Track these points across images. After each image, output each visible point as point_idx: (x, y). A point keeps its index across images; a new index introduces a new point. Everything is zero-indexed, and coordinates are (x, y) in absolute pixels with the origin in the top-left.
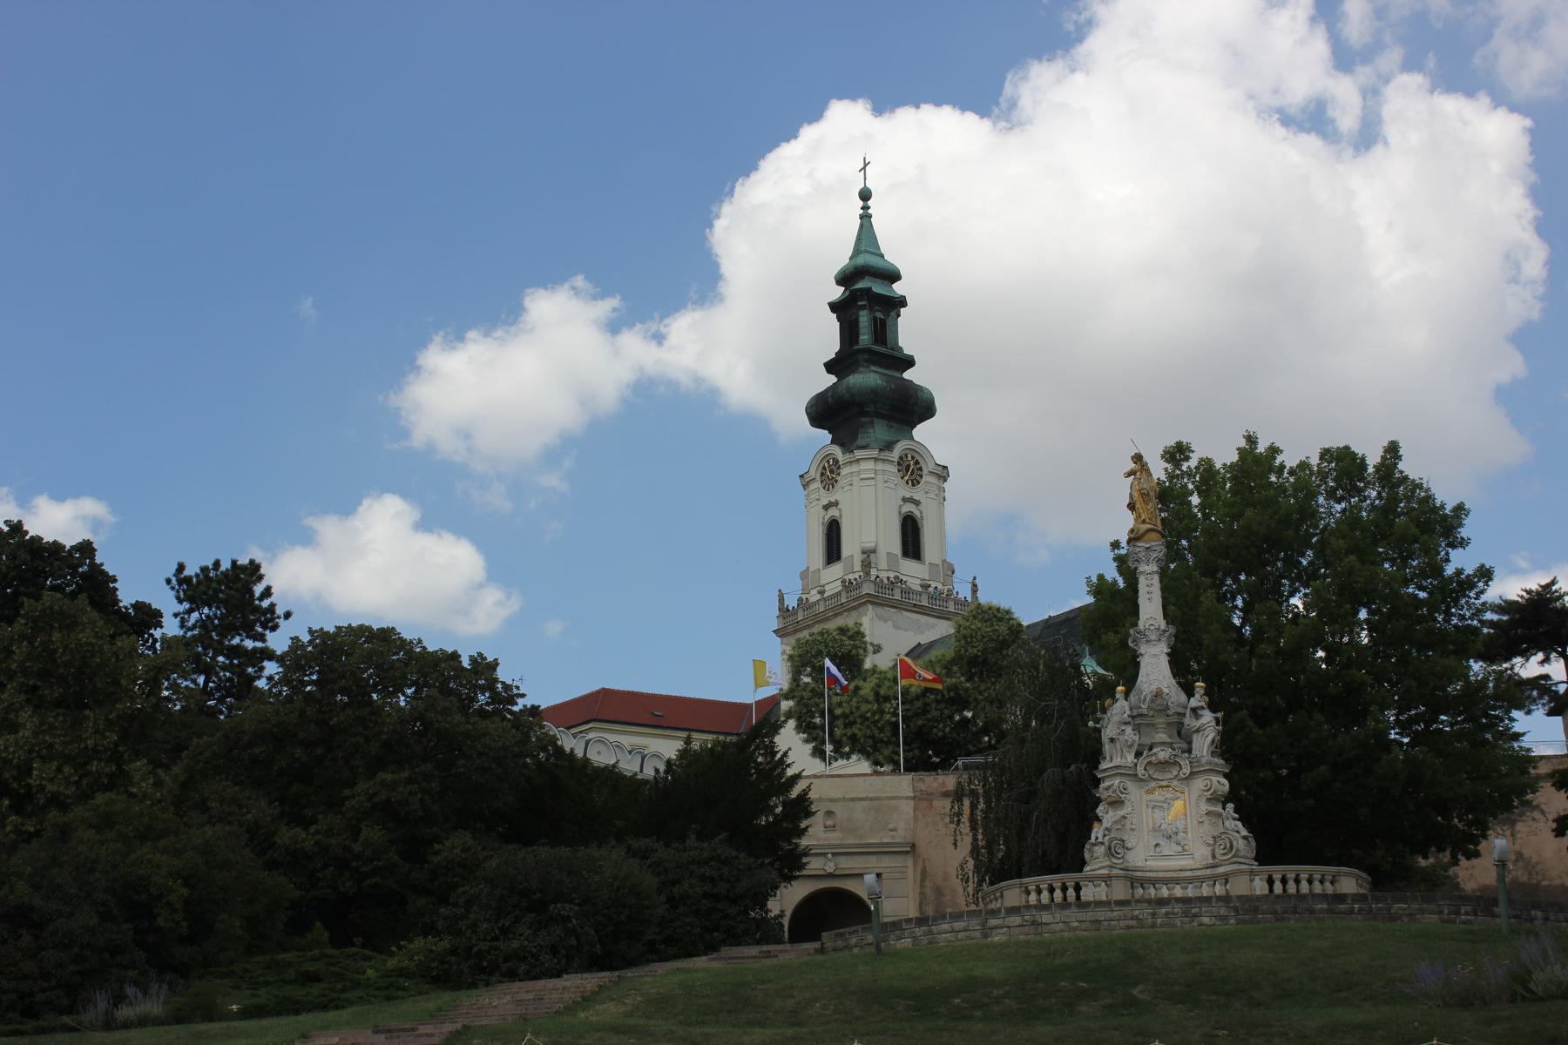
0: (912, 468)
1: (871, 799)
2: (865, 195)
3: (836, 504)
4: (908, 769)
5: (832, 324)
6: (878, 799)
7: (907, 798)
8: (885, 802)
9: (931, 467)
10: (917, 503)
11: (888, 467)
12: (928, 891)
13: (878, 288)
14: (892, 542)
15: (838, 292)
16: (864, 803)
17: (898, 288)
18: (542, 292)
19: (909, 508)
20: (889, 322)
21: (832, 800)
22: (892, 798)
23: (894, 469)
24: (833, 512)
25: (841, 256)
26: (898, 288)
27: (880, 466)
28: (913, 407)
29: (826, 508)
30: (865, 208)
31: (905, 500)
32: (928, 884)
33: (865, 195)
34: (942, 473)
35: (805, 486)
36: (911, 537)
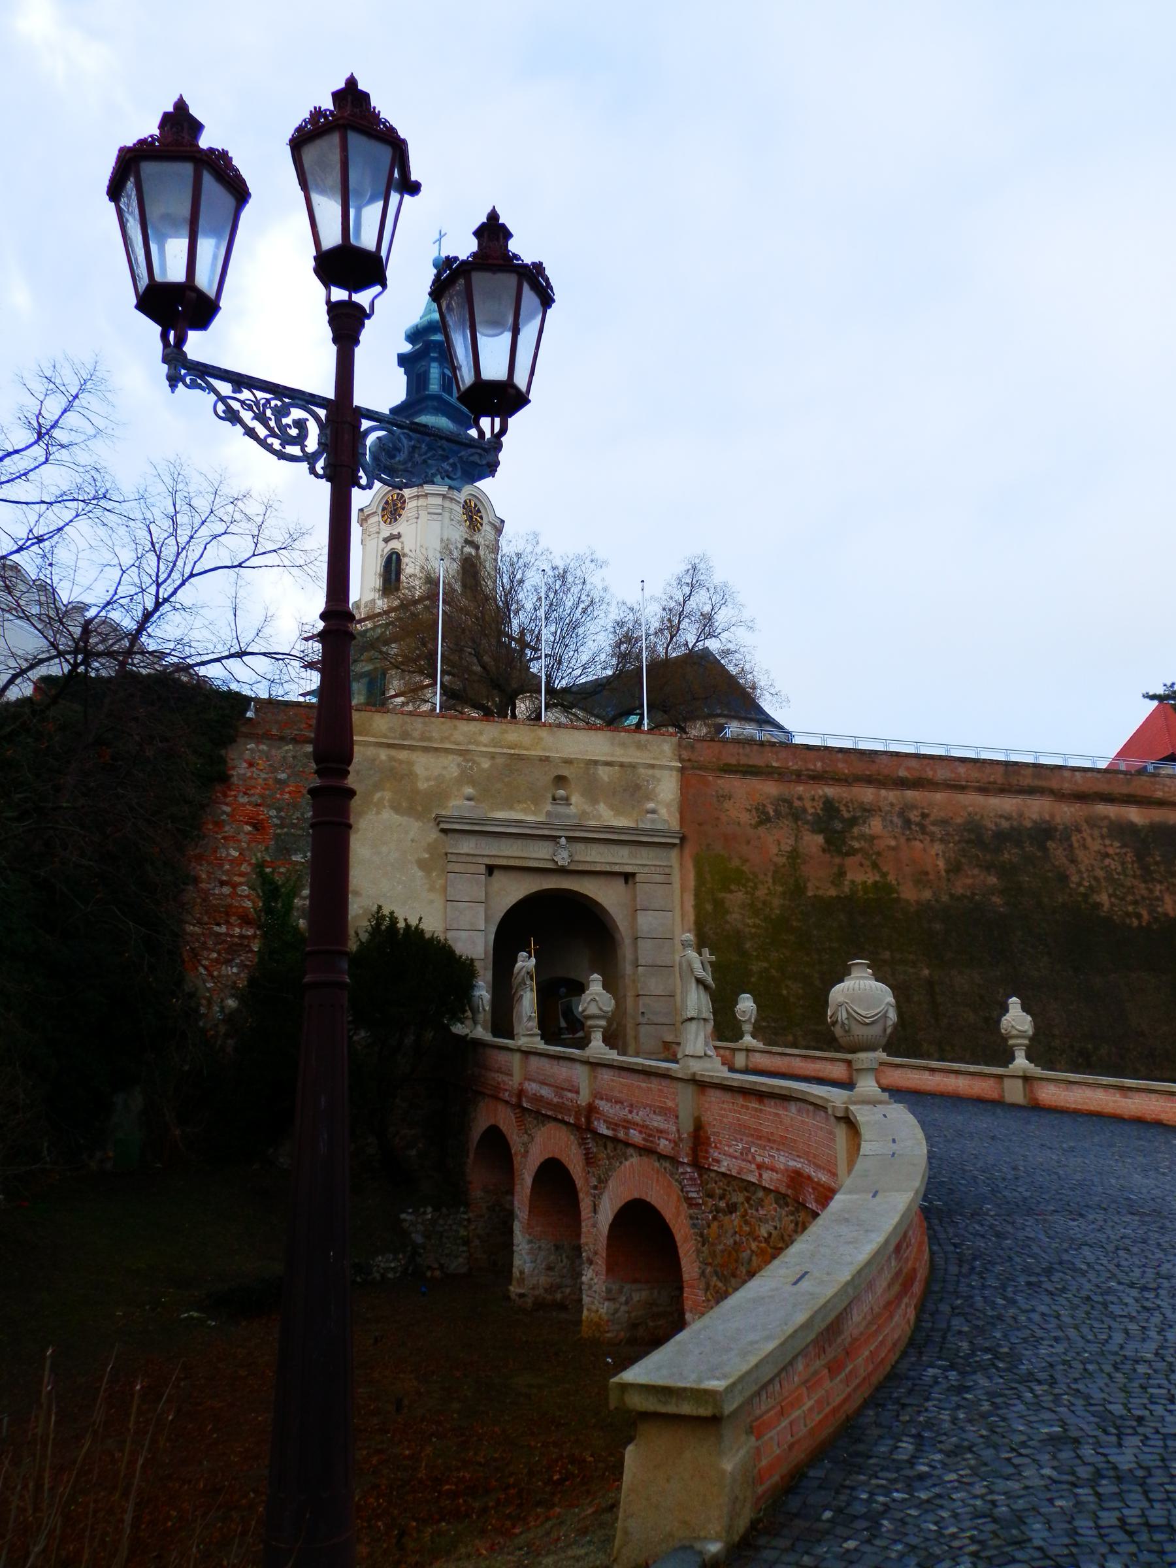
0: (474, 513)
3: (398, 536)
7: (671, 768)
15: (407, 348)
24: (394, 544)
27: (447, 504)
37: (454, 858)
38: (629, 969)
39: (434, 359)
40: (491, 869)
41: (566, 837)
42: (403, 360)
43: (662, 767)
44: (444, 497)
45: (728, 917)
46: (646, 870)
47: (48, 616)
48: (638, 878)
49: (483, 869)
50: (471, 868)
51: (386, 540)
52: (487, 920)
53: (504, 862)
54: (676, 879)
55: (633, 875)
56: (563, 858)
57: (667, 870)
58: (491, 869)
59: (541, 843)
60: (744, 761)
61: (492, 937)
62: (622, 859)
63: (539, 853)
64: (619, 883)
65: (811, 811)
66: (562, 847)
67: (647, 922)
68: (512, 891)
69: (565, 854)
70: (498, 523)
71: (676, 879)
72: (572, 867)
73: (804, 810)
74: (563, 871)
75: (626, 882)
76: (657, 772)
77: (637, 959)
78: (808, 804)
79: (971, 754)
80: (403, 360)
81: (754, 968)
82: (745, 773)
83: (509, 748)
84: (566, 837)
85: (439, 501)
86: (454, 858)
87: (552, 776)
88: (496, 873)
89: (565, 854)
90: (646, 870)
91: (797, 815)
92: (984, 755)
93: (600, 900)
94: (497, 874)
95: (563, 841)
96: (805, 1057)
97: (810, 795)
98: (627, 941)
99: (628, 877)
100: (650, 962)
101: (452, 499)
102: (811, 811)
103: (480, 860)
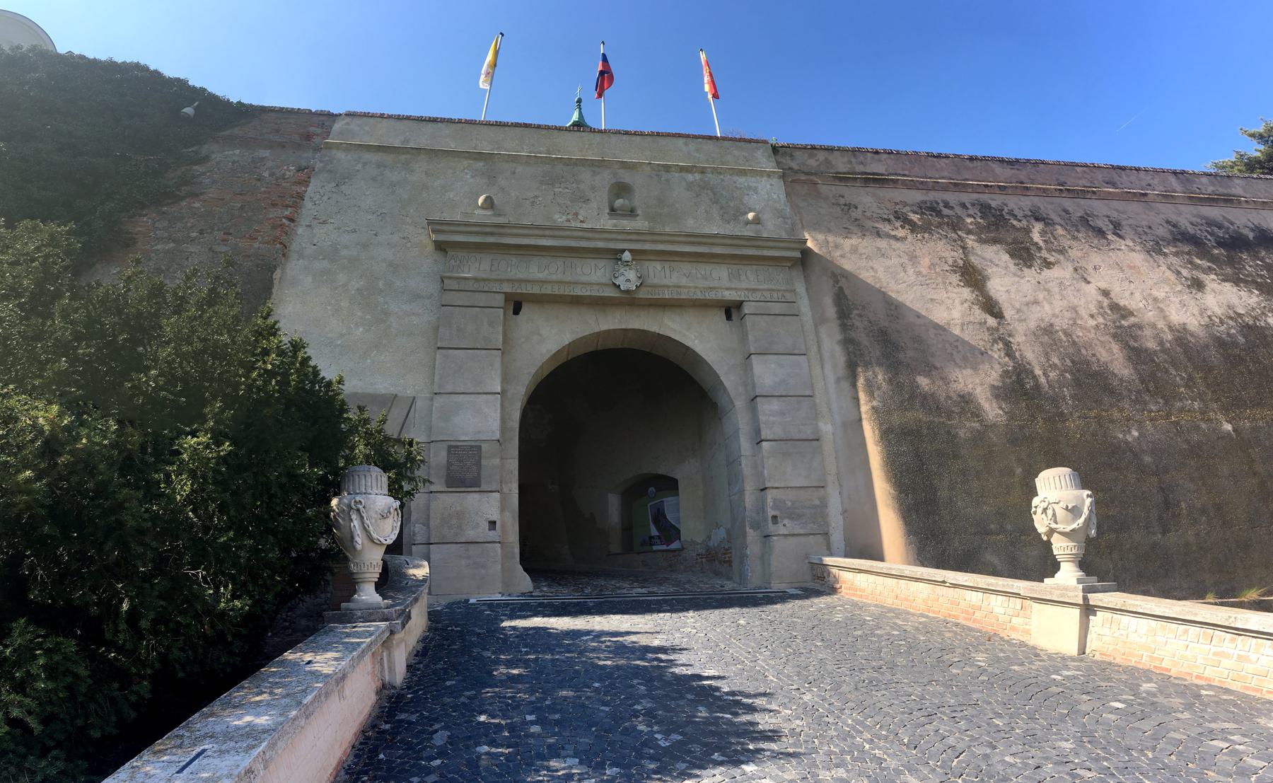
7: (769, 175)
21: (624, 165)
37: (454, 285)
38: (745, 445)
40: (516, 305)
41: (630, 251)
43: (761, 174)
45: (901, 356)
47: (674, 699)
48: (747, 309)
49: (500, 300)
50: (481, 299)
52: (506, 379)
53: (536, 290)
54: (804, 306)
55: (739, 305)
56: (628, 278)
57: (789, 297)
61: (516, 415)
62: (722, 282)
66: (627, 263)
67: (766, 372)
68: (549, 338)
69: (631, 275)
71: (804, 306)
72: (643, 294)
74: (629, 301)
75: (729, 317)
76: (752, 181)
77: (758, 432)
84: (630, 251)
86: (454, 285)
88: (525, 309)
89: (631, 275)
90: (758, 296)
93: (689, 344)
95: (627, 256)
96: (985, 591)
98: (740, 404)
99: (731, 310)
103: (497, 287)
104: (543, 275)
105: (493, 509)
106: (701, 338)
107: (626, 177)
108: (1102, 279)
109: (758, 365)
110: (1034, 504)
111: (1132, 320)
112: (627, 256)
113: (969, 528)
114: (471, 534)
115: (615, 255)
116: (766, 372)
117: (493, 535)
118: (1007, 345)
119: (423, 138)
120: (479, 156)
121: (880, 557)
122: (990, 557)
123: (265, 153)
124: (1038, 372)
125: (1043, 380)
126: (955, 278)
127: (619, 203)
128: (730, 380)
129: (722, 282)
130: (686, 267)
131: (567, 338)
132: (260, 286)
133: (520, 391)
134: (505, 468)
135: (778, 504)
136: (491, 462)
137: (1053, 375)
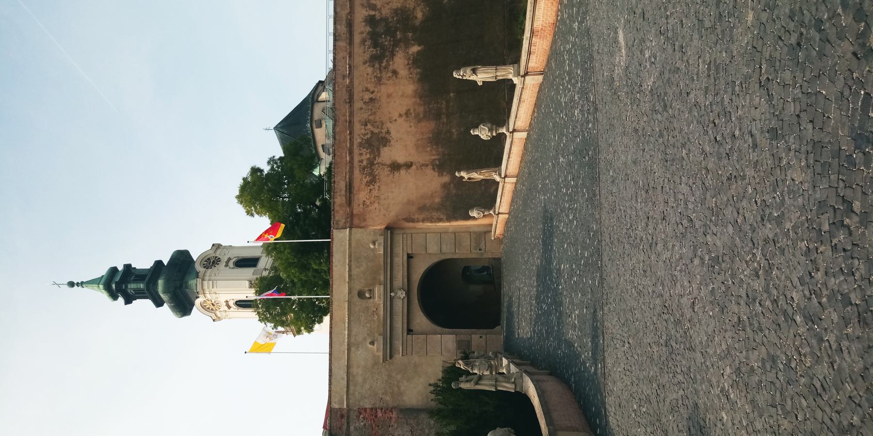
0: (211, 262)
1: (350, 261)
2: (71, 284)
3: (227, 301)
4: (328, 235)
5: (138, 303)
6: (350, 256)
7: (350, 233)
8: (353, 245)
9: (212, 252)
10: (229, 259)
11: (208, 274)
12: (421, 217)
13: (117, 278)
14: (248, 272)
15: (121, 300)
16: (353, 267)
17: (120, 268)
18: (505, 289)
19: (231, 264)
20: (137, 273)
21: (350, 292)
22: (350, 244)
23: (210, 270)
24: (231, 303)
25: (102, 296)
26: (120, 268)
27: (207, 278)
28: (182, 259)
29: (229, 307)
30: (78, 284)
31: (226, 266)
32: (416, 216)
33: (71, 284)
34: (217, 247)
35: (219, 319)
36: (246, 262)
37: (405, 352)
39: (126, 287)
40: (410, 331)
42: (128, 301)
44: (203, 280)
46: (405, 248)
50: (409, 343)
51: (229, 307)
52: (436, 333)
53: (405, 325)
56: (402, 294)
58: (410, 331)
59: (394, 303)
60: (343, 192)
62: (400, 260)
63: (400, 306)
64: (414, 261)
65: (368, 156)
67: (433, 248)
68: (421, 320)
70: (215, 248)
73: (368, 159)
78: (364, 157)
79: (331, 21)
80: (128, 301)
81: (454, 191)
82: (351, 192)
83: (345, 259)
85: (205, 283)
87: (359, 300)
91: (371, 163)
92: (332, 12)
94: (412, 328)
95: (392, 294)
96: (529, 53)
97: (361, 53)
99: (410, 257)
100: (453, 246)
101: (204, 275)
102: (368, 156)
104: (400, 322)
105: (477, 338)
106: (420, 269)
107: (355, 293)
108: (395, 115)
109: (430, 251)
110: (474, 213)
111: (412, 111)
112: (392, 294)
113: (485, 195)
114: (484, 343)
115: (392, 298)
116: (433, 248)
117: (484, 337)
118: (423, 165)
119: (341, 373)
120: (349, 350)
121: (491, 225)
122: (492, 191)
123: (352, 428)
124: (433, 157)
125: (436, 157)
126: (397, 174)
127: (367, 295)
128: (435, 260)
129: (400, 260)
130: (395, 272)
131: (421, 314)
132: (409, 412)
133: (439, 329)
134: (464, 333)
135: (475, 249)
136: (463, 337)
137: (434, 152)
